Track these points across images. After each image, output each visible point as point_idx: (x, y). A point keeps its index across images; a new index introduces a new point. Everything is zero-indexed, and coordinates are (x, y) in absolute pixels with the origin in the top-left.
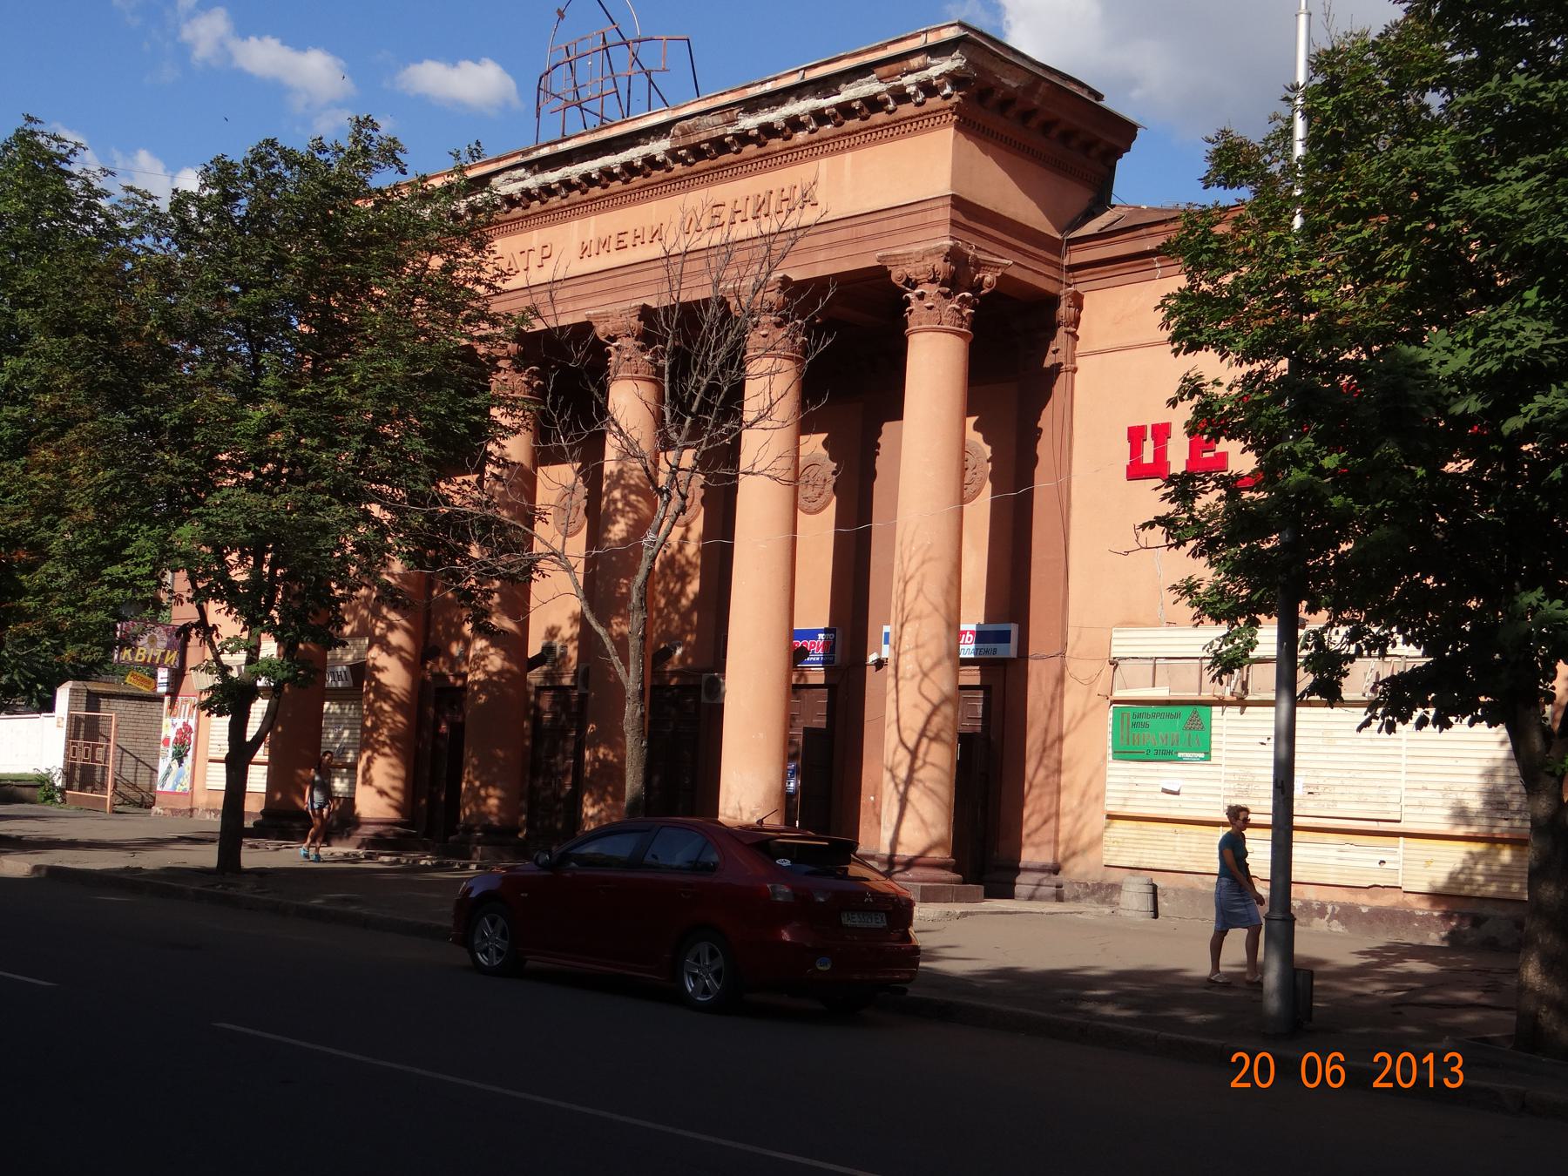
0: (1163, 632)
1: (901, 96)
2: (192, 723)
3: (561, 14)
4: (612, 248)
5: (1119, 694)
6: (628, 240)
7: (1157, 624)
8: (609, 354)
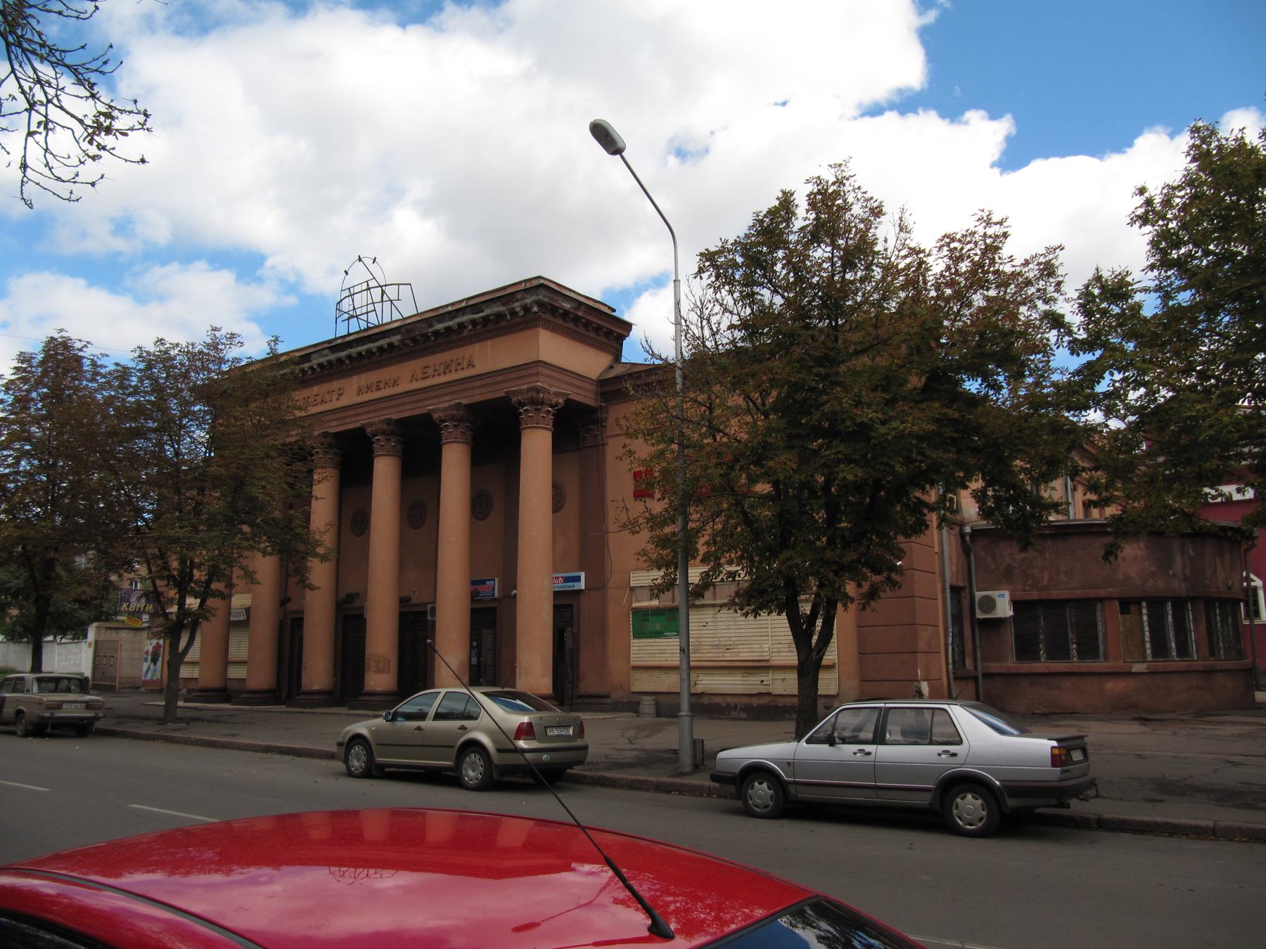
1: (513, 313)
3: (346, 273)
5: (634, 605)
6: (382, 385)
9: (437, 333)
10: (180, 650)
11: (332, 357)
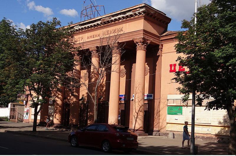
0: (175, 95)
2: (29, 109)
3: (84, 2)
4: (92, 37)
5: (168, 105)
6: (95, 36)
7: (174, 94)
8: (137, 46)
9: (112, 21)
10: (190, 134)
11: (80, 27)
